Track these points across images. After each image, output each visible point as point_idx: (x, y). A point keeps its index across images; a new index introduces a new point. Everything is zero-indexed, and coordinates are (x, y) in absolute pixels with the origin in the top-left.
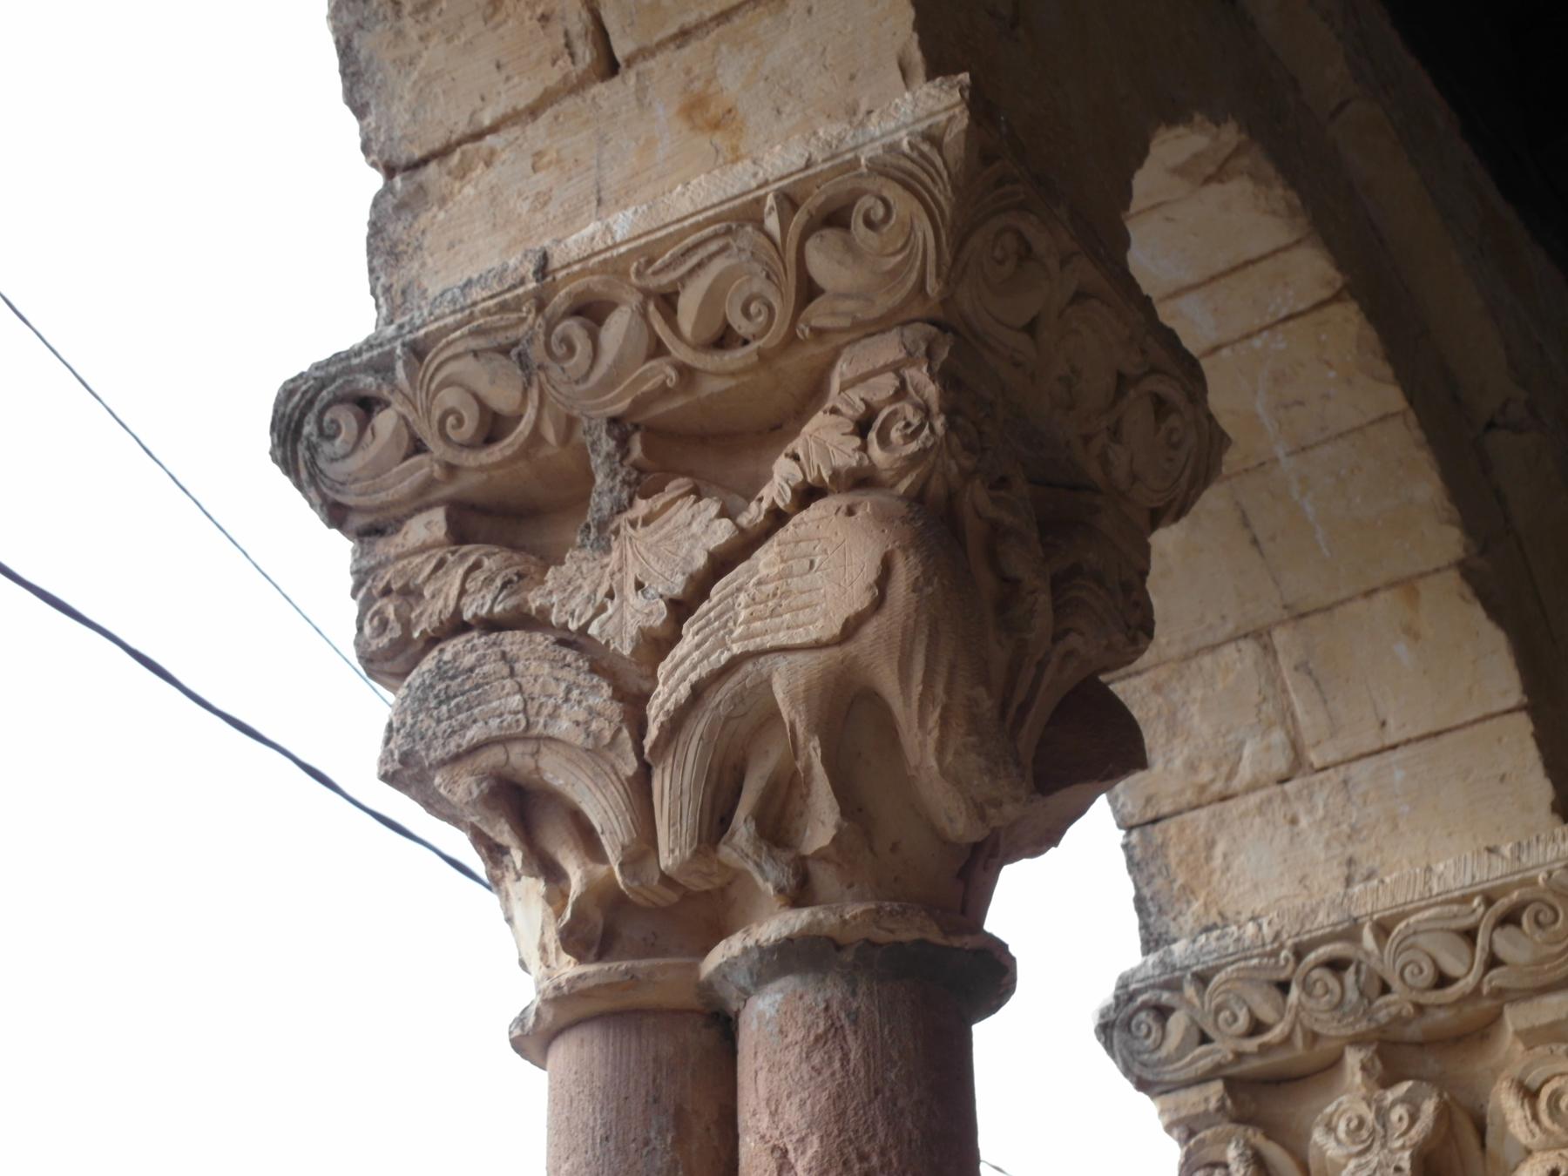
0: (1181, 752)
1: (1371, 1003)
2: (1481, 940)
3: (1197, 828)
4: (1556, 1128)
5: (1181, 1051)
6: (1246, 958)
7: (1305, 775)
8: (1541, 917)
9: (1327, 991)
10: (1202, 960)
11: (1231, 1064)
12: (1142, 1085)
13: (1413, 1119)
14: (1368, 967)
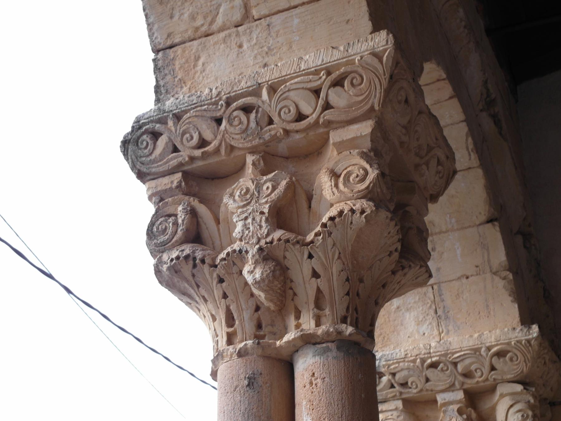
0: (189, 10)
1: (262, 129)
2: (323, 95)
3: (192, 50)
4: (346, 190)
5: (162, 155)
6: (201, 106)
7: (249, 22)
8: (354, 81)
9: (241, 123)
10: (179, 107)
11: (187, 163)
12: (141, 176)
13: (274, 188)
14: (263, 109)
